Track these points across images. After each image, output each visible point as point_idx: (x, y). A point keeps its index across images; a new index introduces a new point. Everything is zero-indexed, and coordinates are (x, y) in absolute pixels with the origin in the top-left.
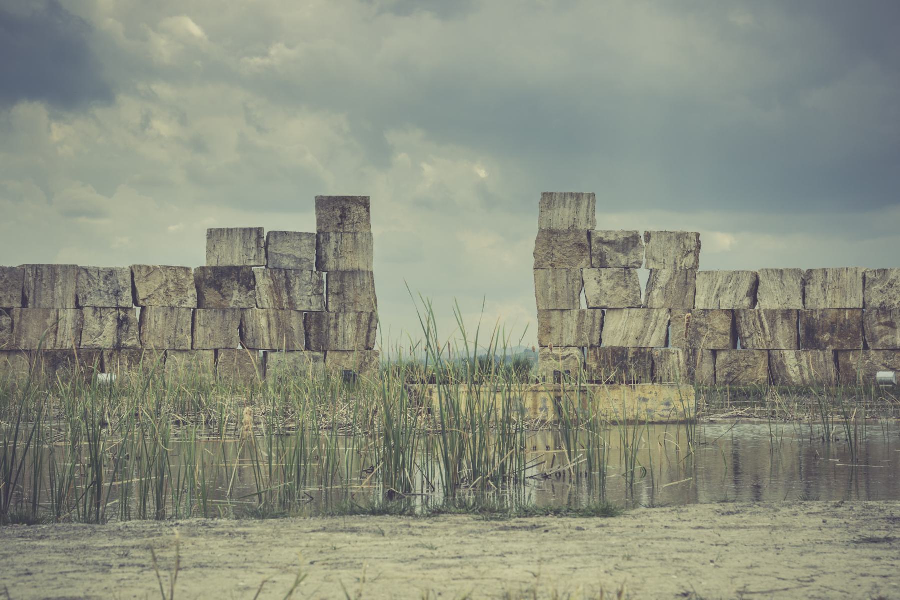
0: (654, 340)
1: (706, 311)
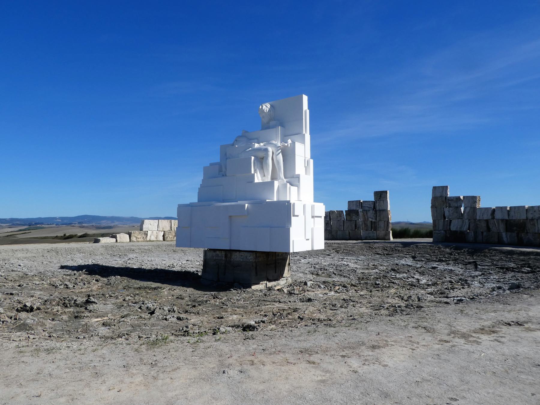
0: (465, 228)
1: (479, 220)
